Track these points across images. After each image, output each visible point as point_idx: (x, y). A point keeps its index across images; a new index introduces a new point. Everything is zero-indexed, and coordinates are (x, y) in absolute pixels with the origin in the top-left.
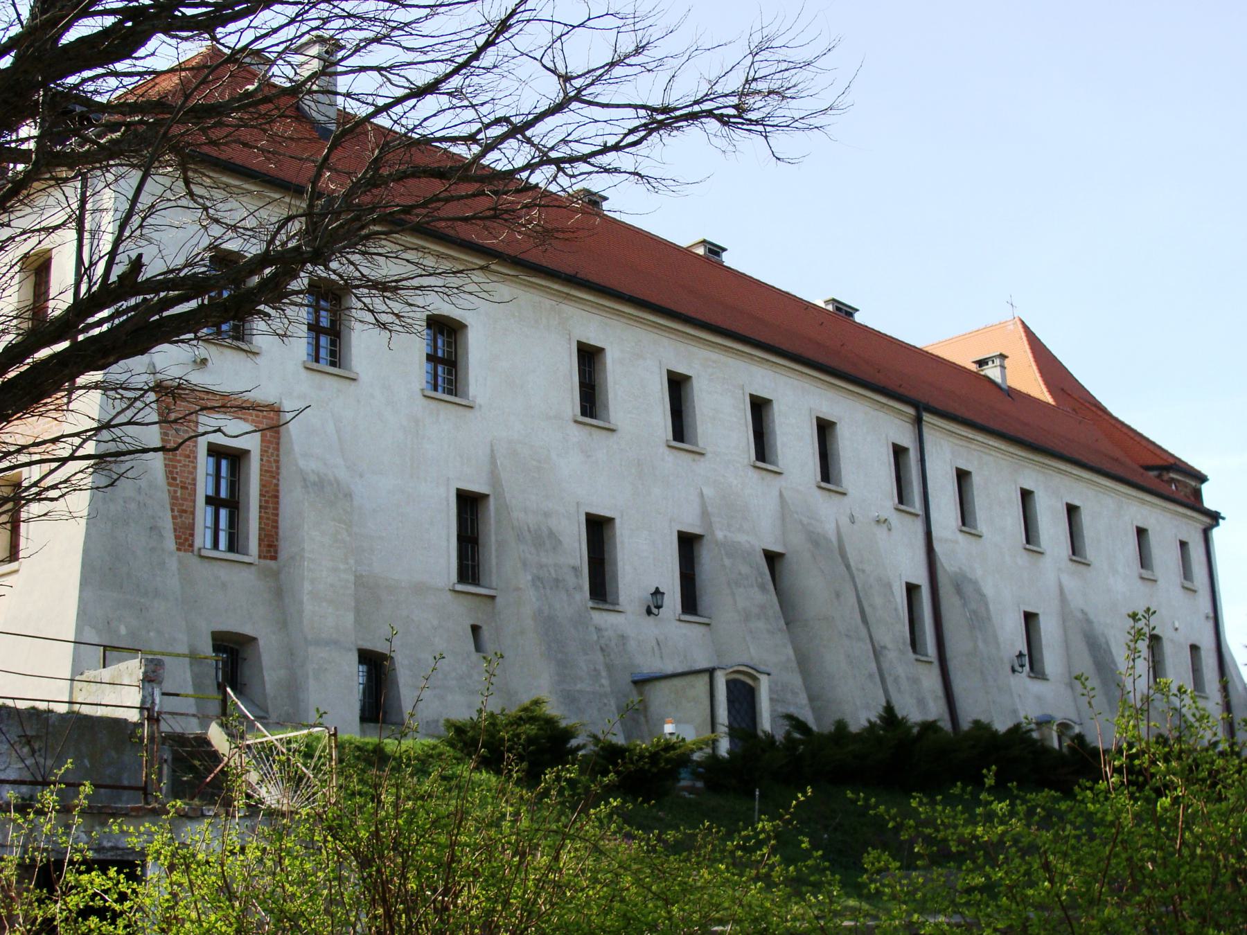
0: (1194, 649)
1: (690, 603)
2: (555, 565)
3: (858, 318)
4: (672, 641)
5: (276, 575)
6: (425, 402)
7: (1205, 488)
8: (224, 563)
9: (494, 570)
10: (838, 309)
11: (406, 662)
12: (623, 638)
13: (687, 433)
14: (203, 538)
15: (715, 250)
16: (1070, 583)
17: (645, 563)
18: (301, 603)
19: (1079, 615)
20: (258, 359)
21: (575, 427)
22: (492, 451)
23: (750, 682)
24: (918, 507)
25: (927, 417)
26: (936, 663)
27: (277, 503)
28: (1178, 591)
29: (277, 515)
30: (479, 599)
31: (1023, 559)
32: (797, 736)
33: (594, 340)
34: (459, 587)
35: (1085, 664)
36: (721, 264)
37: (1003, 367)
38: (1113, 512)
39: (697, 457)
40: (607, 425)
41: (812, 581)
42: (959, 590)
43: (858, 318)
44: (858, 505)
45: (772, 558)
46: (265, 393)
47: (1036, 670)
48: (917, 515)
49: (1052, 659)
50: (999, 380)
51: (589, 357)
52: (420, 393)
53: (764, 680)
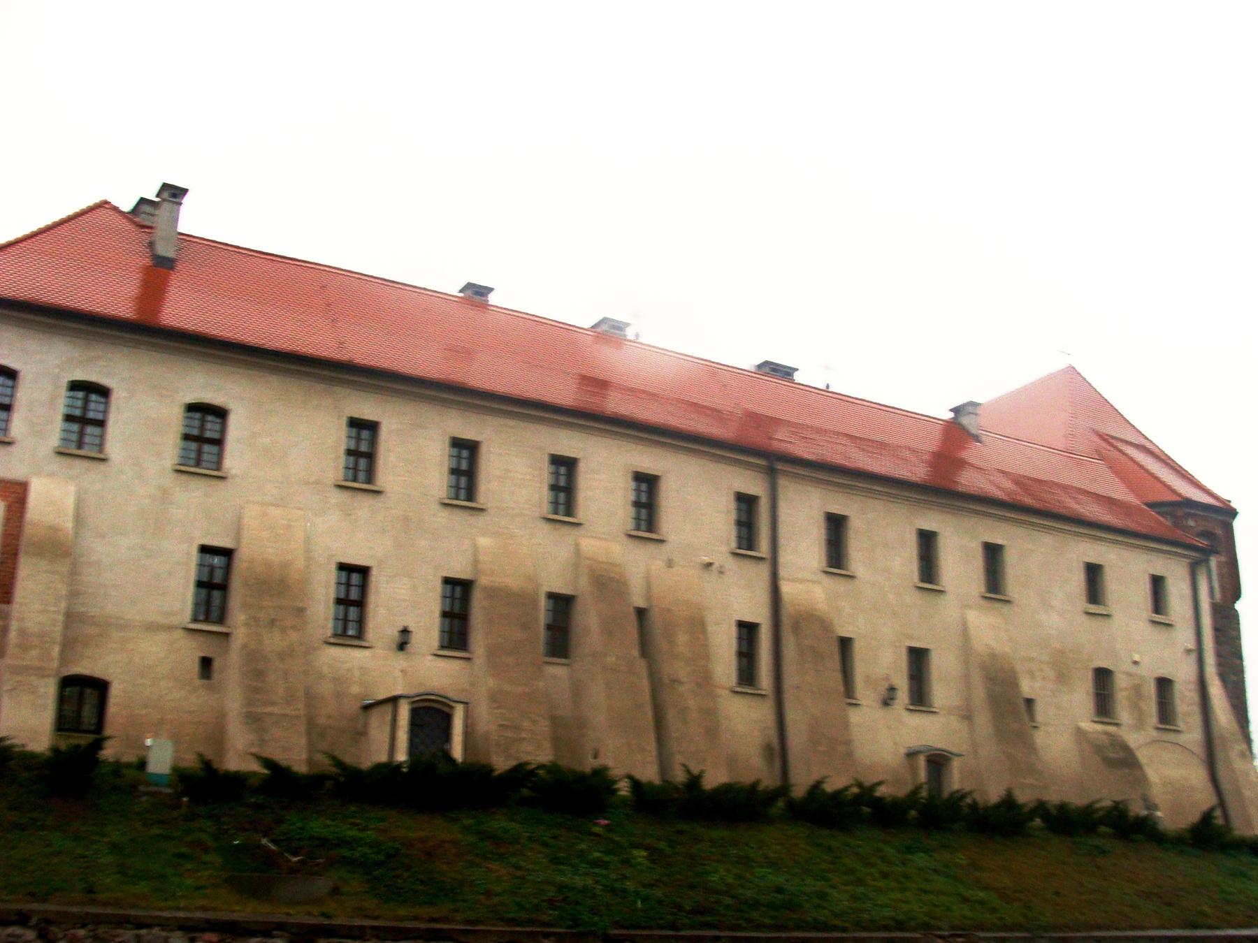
7: (1238, 524)
21: (546, 527)
23: (446, 709)
31: (912, 598)
47: (920, 697)
49: (942, 692)
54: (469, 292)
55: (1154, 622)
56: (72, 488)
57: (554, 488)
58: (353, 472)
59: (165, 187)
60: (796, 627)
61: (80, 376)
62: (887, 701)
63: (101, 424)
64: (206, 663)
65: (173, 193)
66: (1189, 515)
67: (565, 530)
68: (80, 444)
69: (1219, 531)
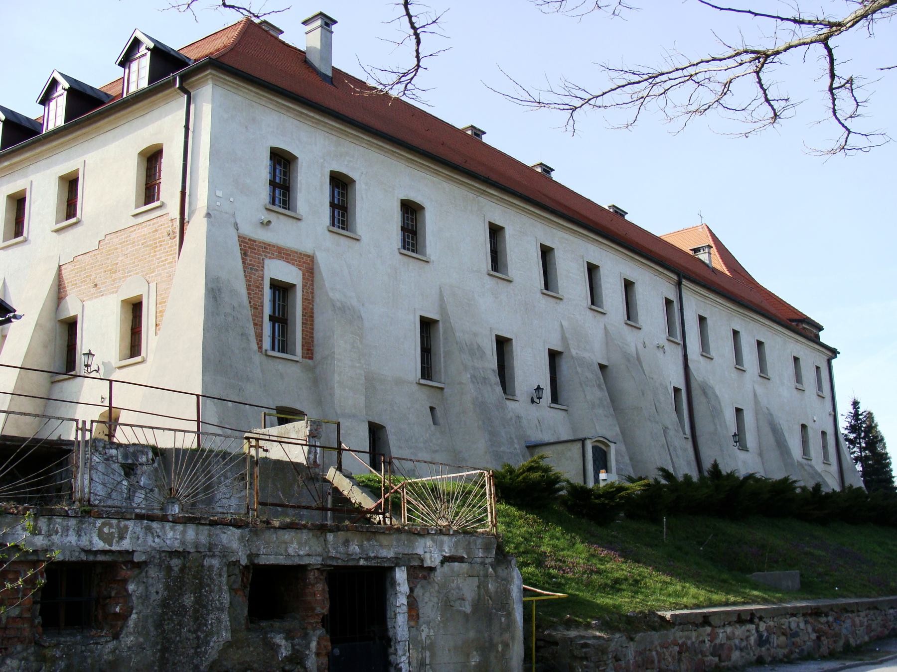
0: (824, 433)
1: (555, 398)
2: (483, 368)
3: (627, 217)
4: (546, 422)
5: (312, 369)
6: (401, 257)
7: (821, 333)
8: (281, 361)
9: (443, 370)
11: (393, 431)
12: (519, 417)
14: (267, 344)
15: (548, 170)
16: (760, 391)
17: (530, 370)
18: (332, 388)
19: (765, 410)
20: (301, 224)
22: (441, 291)
23: (603, 447)
24: (679, 339)
25: (684, 282)
26: (690, 439)
27: (313, 321)
28: (815, 397)
29: (313, 329)
30: (432, 390)
31: (734, 374)
32: (663, 482)
33: (499, 222)
34: (422, 381)
35: (770, 440)
36: (551, 179)
37: (709, 253)
38: (782, 346)
39: (558, 301)
40: (507, 278)
41: (628, 385)
42: (705, 393)
44: (643, 334)
45: (602, 367)
46: (306, 247)
48: (678, 344)
49: (750, 439)
50: (707, 262)
51: (495, 232)
52: (397, 251)
53: (612, 446)
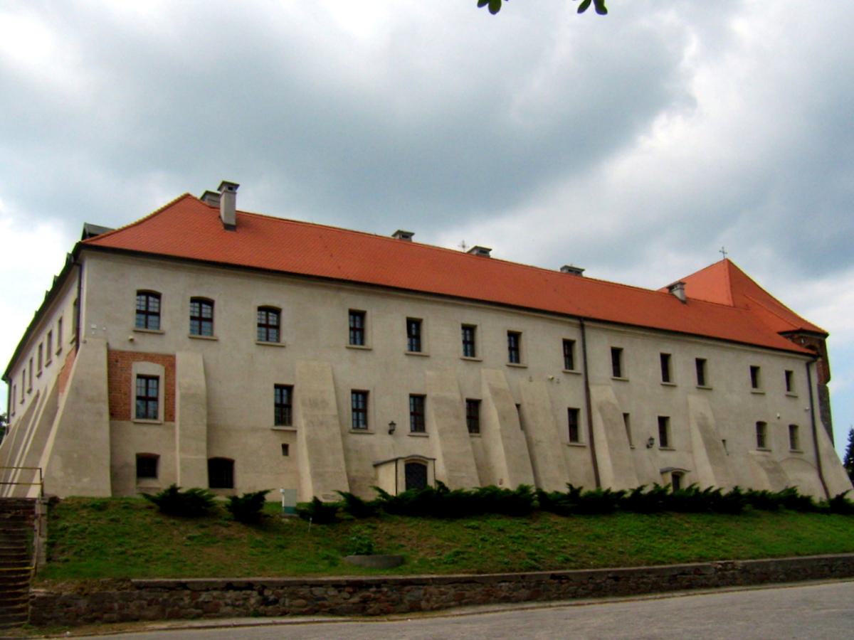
0: (793, 428)
7: (828, 340)
10: (570, 271)
13: (759, 384)
23: (423, 463)
31: (660, 390)
43: (585, 274)
54: (565, 271)
55: (754, 393)
56: (200, 357)
57: (465, 342)
58: (354, 340)
59: (224, 183)
60: (601, 409)
61: (196, 294)
62: (649, 445)
63: (211, 320)
64: (285, 448)
65: (231, 187)
66: (802, 337)
67: (472, 365)
68: (146, 326)
69: (817, 346)
